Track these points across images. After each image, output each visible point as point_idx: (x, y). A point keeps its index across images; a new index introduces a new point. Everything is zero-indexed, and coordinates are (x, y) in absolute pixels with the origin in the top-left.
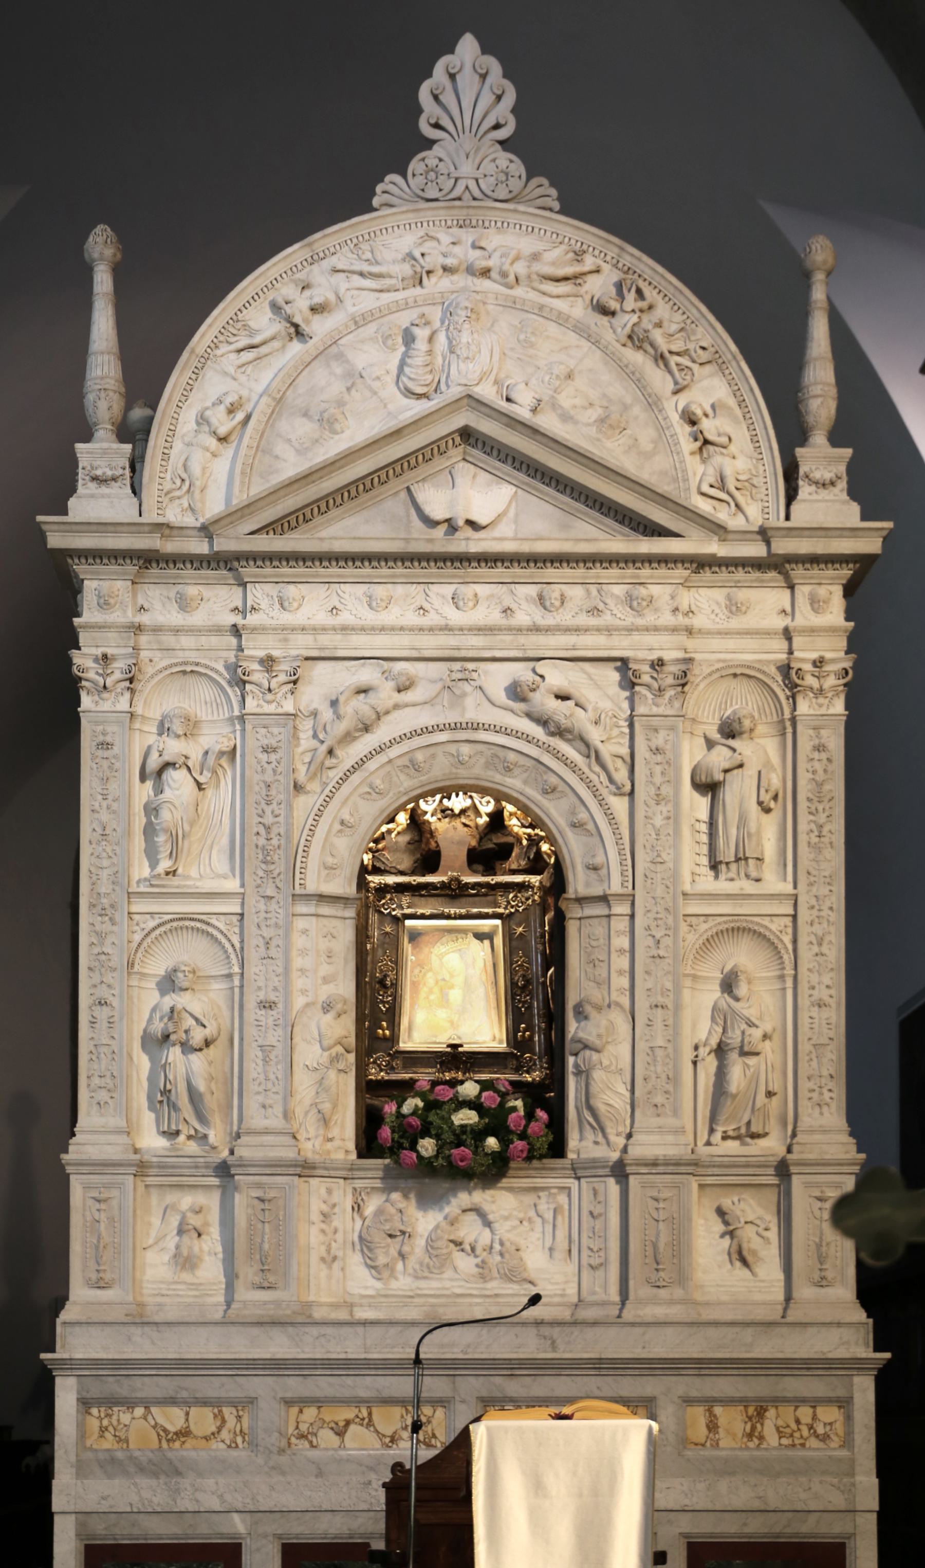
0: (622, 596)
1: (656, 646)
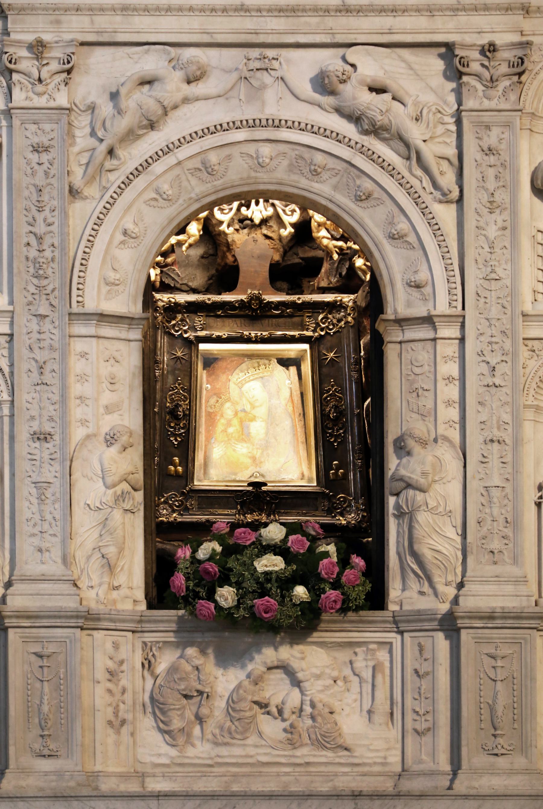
1: (487, 28)
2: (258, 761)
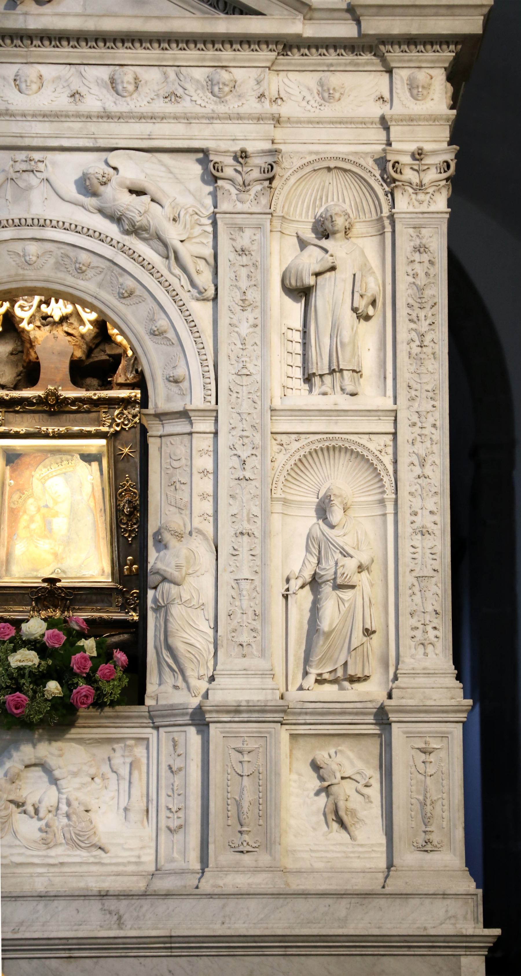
0: (202, 80)
1: (240, 135)
2: (12, 862)
